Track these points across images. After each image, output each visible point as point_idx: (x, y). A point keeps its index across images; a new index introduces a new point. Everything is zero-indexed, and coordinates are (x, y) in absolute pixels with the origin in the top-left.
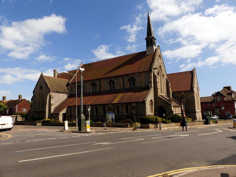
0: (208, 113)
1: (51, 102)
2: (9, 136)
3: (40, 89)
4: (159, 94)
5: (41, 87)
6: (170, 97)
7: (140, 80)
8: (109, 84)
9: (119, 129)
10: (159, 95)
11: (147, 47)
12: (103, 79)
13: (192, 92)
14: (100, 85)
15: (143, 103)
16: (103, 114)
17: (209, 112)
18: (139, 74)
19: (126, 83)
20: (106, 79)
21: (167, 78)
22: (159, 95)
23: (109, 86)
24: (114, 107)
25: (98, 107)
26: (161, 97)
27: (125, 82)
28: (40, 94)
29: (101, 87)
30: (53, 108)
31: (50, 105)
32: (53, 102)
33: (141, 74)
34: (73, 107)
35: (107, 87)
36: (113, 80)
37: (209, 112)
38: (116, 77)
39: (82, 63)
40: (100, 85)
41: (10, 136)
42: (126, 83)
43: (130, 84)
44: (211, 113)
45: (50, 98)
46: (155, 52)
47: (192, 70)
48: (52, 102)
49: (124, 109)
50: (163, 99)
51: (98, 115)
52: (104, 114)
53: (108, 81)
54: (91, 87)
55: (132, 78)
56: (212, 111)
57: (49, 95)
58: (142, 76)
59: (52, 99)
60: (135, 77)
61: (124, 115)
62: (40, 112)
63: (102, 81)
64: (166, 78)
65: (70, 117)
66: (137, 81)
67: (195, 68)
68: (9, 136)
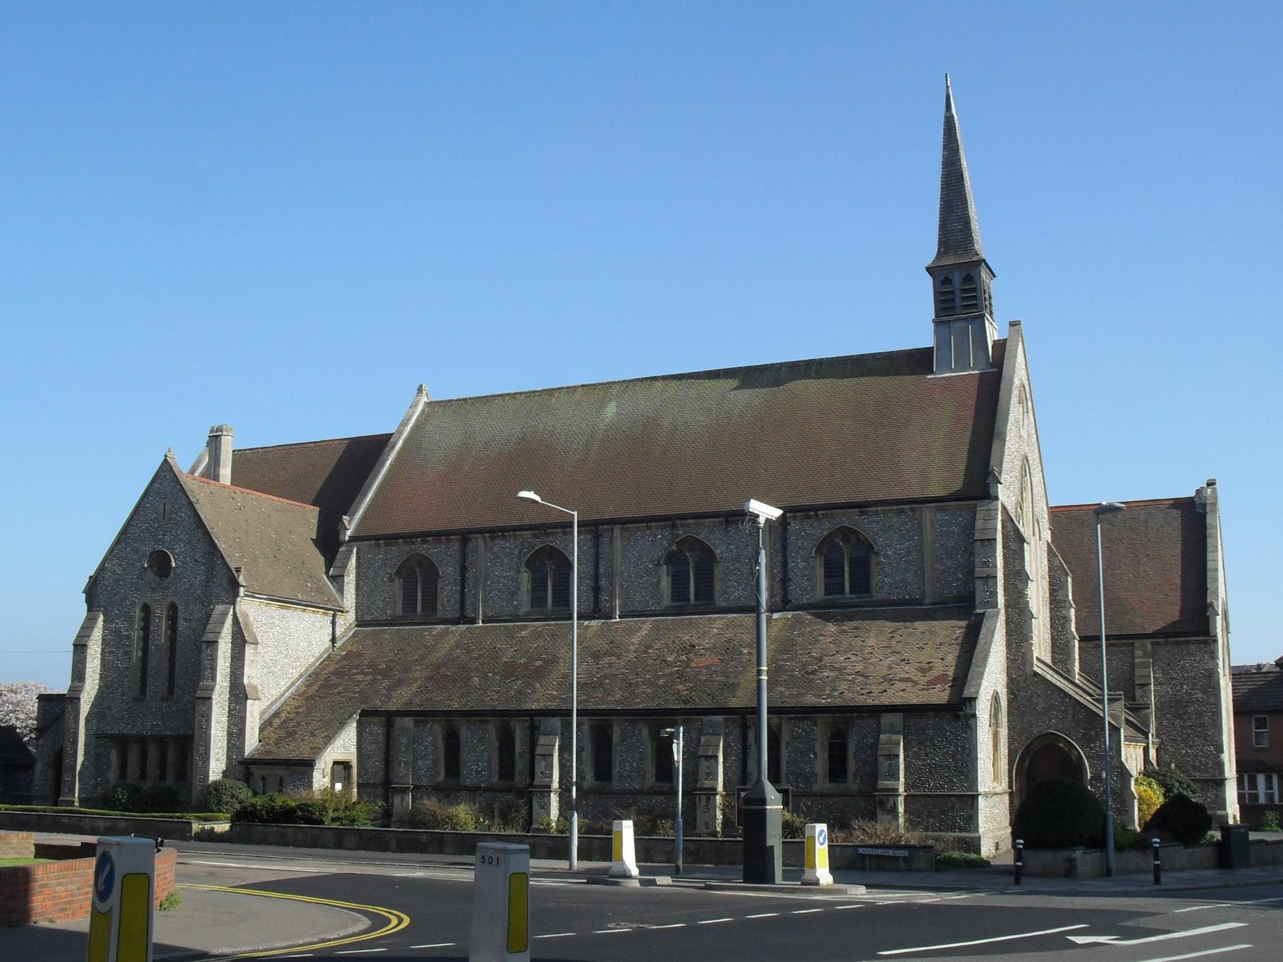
0: (1244, 794)
1: (247, 671)
2: (394, 921)
3: (150, 575)
4: (1035, 655)
5: (160, 564)
6: (1067, 676)
7: (909, 553)
8: (668, 562)
9: (612, 887)
10: (1035, 661)
11: (937, 323)
12: (623, 530)
13: (1205, 642)
14: (596, 567)
15: (957, 718)
16: (650, 781)
17: (1261, 779)
18: (902, 511)
19: (801, 565)
20: (648, 528)
21: (1050, 541)
22: (1038, 659)
23: (665, 582)
24: (737, 731)
25: (611, 727)
26: (1049, 677)
27: (797, 563)
28: (181, 608)
29: (603, 582)
30: (255, 713)
31: (239, 695)
32: (253, 673)
33: (912, 510)
34: (408, 722)
35: (659, 582)
36: (701, 537)
37: (1261, 779)
38: (727, 522)
39: (420, 390)
40: (596, 567)
41: (401, 921)
42: (801, 565)
43: (828, 575)
44: (1269, 785)
45: (240, 641)
46: (992, 365)
47: (1193, 495)
48: (251, 675)
49: (818, 749)
50: (1058, 684)
51: (616, 784)
52: (658, 780)
53: (661, 541)
54: (525, 578)
55: (847, 533)
56: (1277, 772)
57: (229, 621)
58: (920, 525)
59: (249, 650)
60: (869, 526)
61: (816, 788)
62: (142, 741)
63: (618, 543)
64: (1048, 544)
65: (380, 791)
66: (886, 556)
67: (1211, 484)
68: (394, 921)
